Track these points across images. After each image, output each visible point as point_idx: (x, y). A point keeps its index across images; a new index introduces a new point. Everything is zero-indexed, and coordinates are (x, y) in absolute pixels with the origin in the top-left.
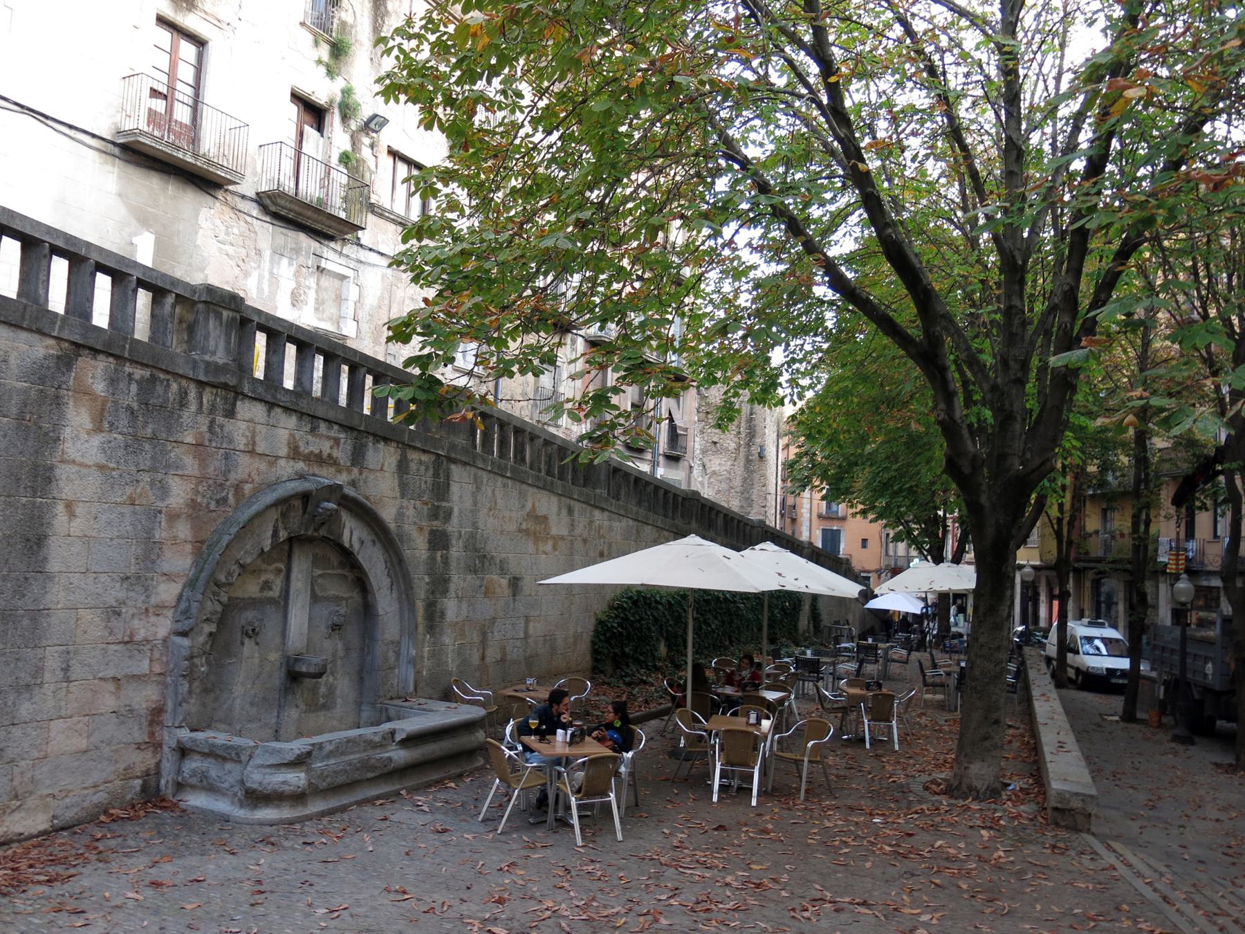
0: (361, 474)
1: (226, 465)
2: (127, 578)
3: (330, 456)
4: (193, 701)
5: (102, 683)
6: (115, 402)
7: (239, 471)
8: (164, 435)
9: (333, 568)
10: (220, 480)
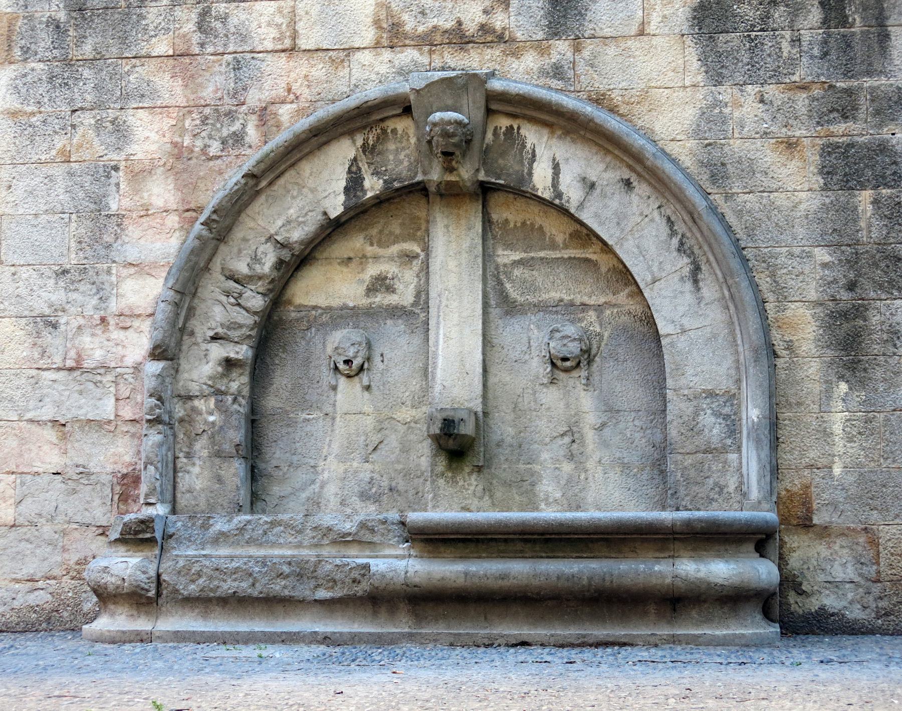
0: (577, 49)
1: (237, 79)
2: (65, 272)
3: (484, 28)
4: (196, 470)
5: (34, 428)
6: (30, 18)
7: (266, 86)
8: (114, 50)
9: (553, 246)
10: (228, 104)
